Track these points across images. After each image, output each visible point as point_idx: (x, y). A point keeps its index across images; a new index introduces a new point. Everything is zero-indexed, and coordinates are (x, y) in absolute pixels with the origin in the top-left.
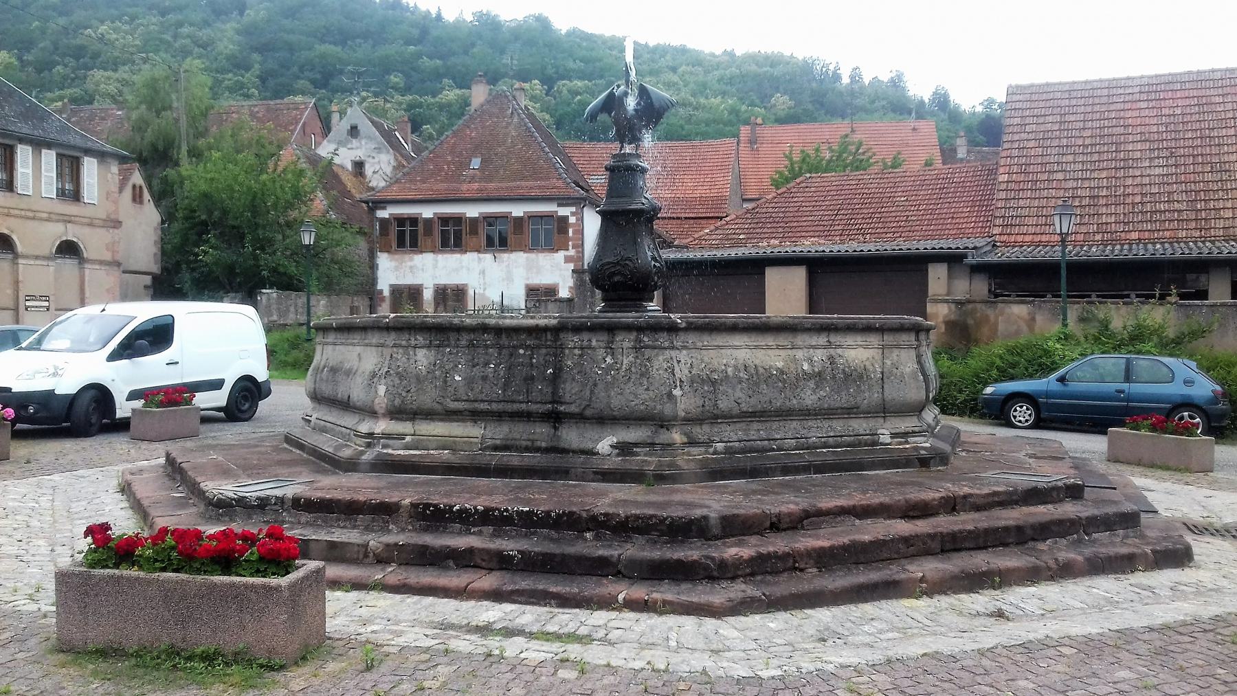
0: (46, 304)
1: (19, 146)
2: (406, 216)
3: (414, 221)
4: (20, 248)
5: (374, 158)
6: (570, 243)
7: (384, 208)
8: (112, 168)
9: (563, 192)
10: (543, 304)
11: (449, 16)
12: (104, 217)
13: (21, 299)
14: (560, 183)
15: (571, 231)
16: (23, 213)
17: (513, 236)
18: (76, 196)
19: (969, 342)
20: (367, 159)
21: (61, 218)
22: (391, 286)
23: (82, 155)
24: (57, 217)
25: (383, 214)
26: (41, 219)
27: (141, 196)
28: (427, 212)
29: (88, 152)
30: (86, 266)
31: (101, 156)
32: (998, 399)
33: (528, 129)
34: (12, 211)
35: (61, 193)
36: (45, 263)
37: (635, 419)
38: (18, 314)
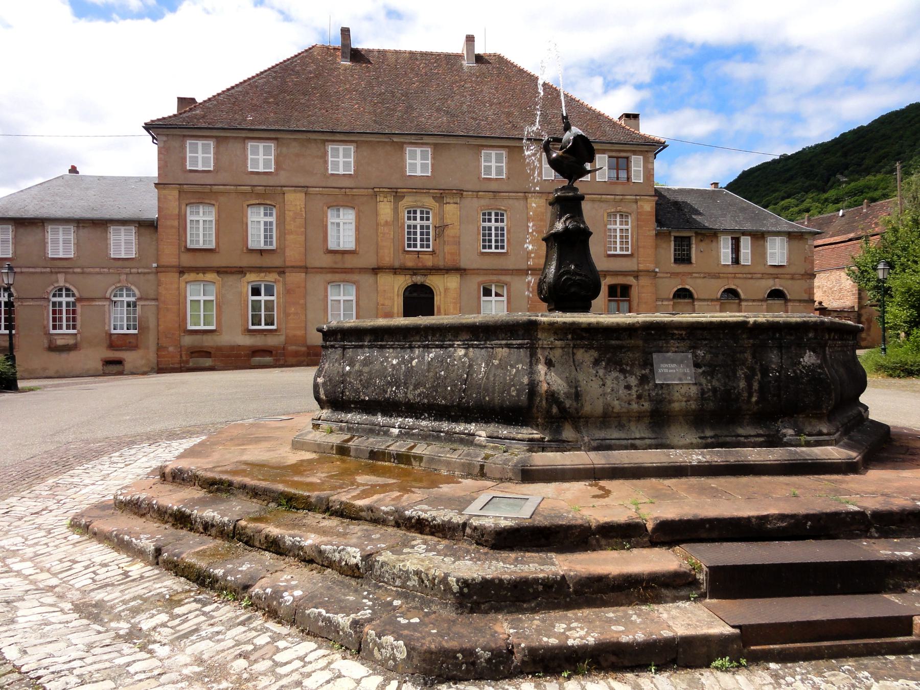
1: (742, 237)
16: (745, 276)
19: (176, 520)
32: (842, 462)
37: (441, 269)
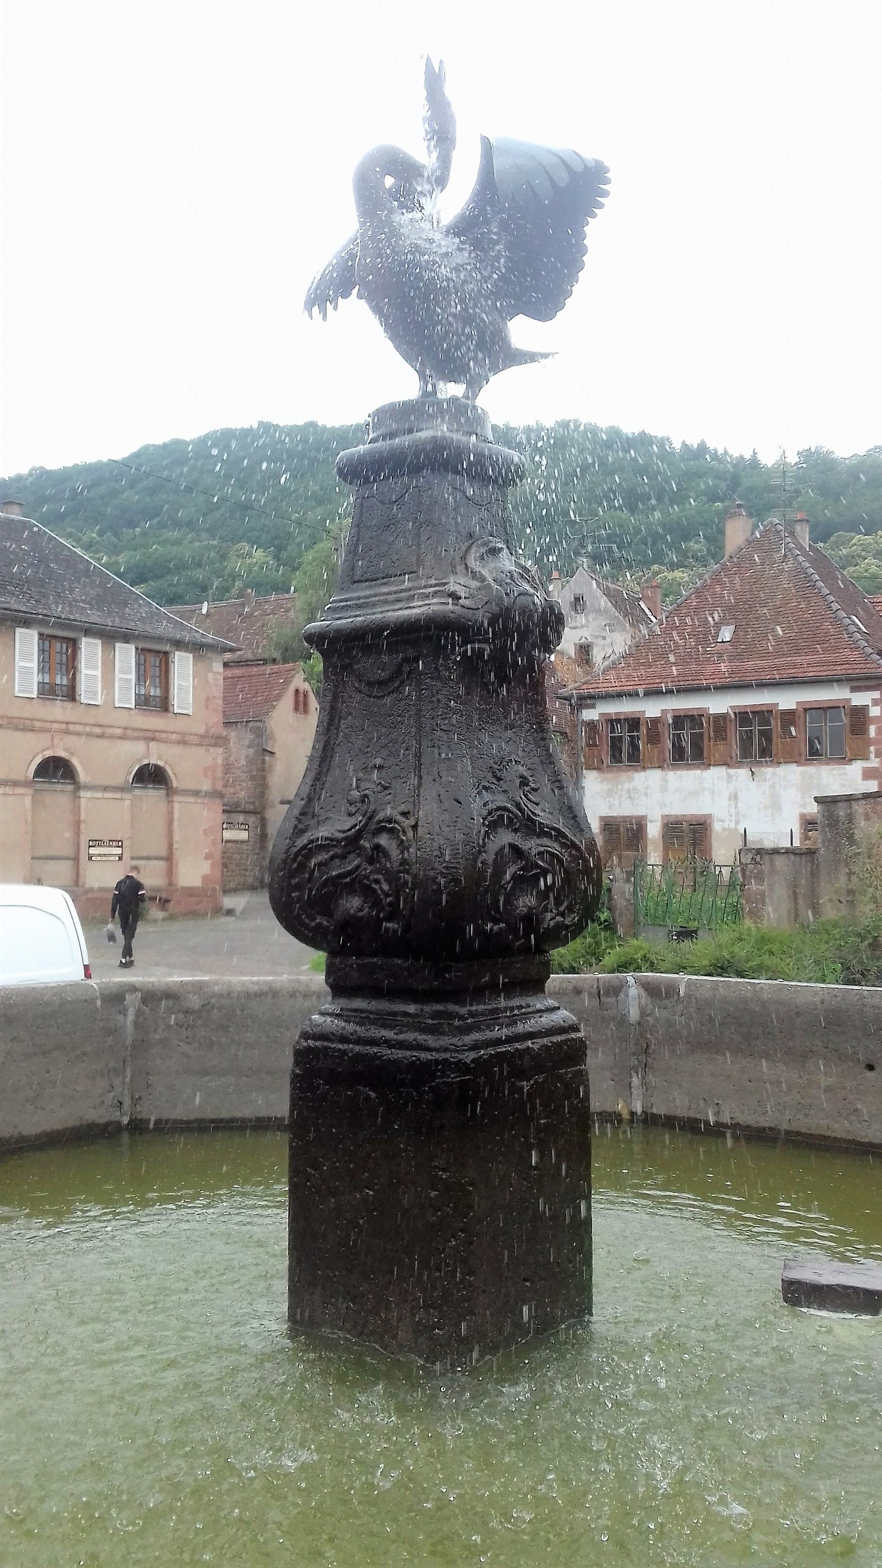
0: (118, 851)
2: (682, 714)
3: (634, 723)
4: (83, 776)
5: (604, 638)
6: (872, 748)
7: (593, 706)
8: (214, 664)
9: (859, 670)
10: (767, 857)
11: (768, 459)
12: (202, 731)
13: (84, 845)
14: (855, 656)
15: (872, 731)
17: (779, 740)
18: (164, 705)
20: (595, 641)
21: (141, 734)
22: (602, 818)
23: (173, 649)
24: (136, 734)
25: (590, 715)
26: (112, 737)
27: (306, 704)
28: (652, 709)
29: (179, 644)
30: (176, 798)
31: (198, 648)
33: (808, 577)
34: (71, 727)
35: (143, 702)
36: (118, 795)
38: (78, 866)
